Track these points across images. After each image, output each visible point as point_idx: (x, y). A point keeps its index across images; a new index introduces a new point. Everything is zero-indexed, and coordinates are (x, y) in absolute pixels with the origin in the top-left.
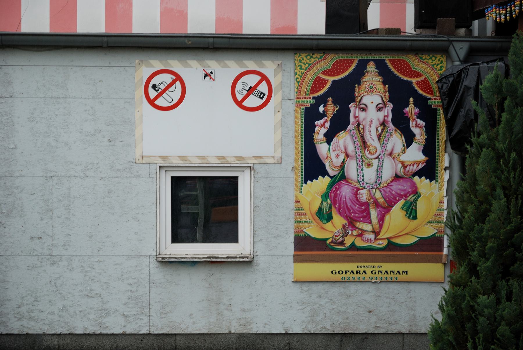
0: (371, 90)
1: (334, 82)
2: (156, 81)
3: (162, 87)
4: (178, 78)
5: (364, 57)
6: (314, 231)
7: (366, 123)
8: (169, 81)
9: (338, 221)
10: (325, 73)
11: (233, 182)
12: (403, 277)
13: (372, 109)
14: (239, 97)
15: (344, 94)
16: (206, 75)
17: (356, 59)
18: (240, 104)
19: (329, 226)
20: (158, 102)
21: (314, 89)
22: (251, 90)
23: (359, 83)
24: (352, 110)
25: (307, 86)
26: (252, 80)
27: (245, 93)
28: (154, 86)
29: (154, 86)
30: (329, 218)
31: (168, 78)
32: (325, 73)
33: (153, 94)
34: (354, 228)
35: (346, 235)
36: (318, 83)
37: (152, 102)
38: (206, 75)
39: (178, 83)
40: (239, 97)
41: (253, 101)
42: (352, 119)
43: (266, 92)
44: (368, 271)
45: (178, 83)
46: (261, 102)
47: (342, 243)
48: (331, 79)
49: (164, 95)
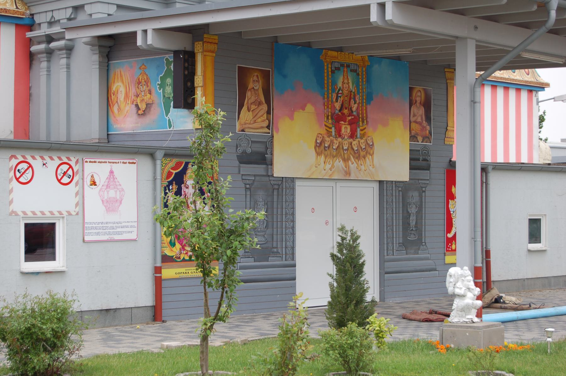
0: (191, 178)
1: (176, 173)
2: (19, 167)
3: (23, 171)
4: (30, 166)
5: (187, 160)
6: (168, 253)
7: (188, 195)
8: (26, 168)
9: (178, 246)
10: (173, 169)
11: (52, 227)
12: (185, 276)
13: (190, 187)
14: (59, 177)
15: (178, 180)
16: (44, 164)
17: (184, 160)
18: (59, 181)
19: (174, 249)
20: (21, 180)
21: (168, 178)
22: (65, 173)
23: (185, 174)
24: (183, 188)
25: (165, 175)
26: (65, 167)
27: (62, 175)
28: (19, 170)
29: (19, 170)
30: (174, 245)
31: (25, 166)
32: (173, 169)
33: (18, 175)
34: (184, 250)
35: (181, 253)
36: (170, 174)
37: (17, 179)
38: (44, 164)
39: (30, 168)
40: (59, 177)
41: (66, 180)
42: (183, 193)
43: (72, 175)
44: (190, 272)
45: (30, 168)
46: (69, 180)
47: (179, 258)
48: (174, 172)
49: (24, 175)
